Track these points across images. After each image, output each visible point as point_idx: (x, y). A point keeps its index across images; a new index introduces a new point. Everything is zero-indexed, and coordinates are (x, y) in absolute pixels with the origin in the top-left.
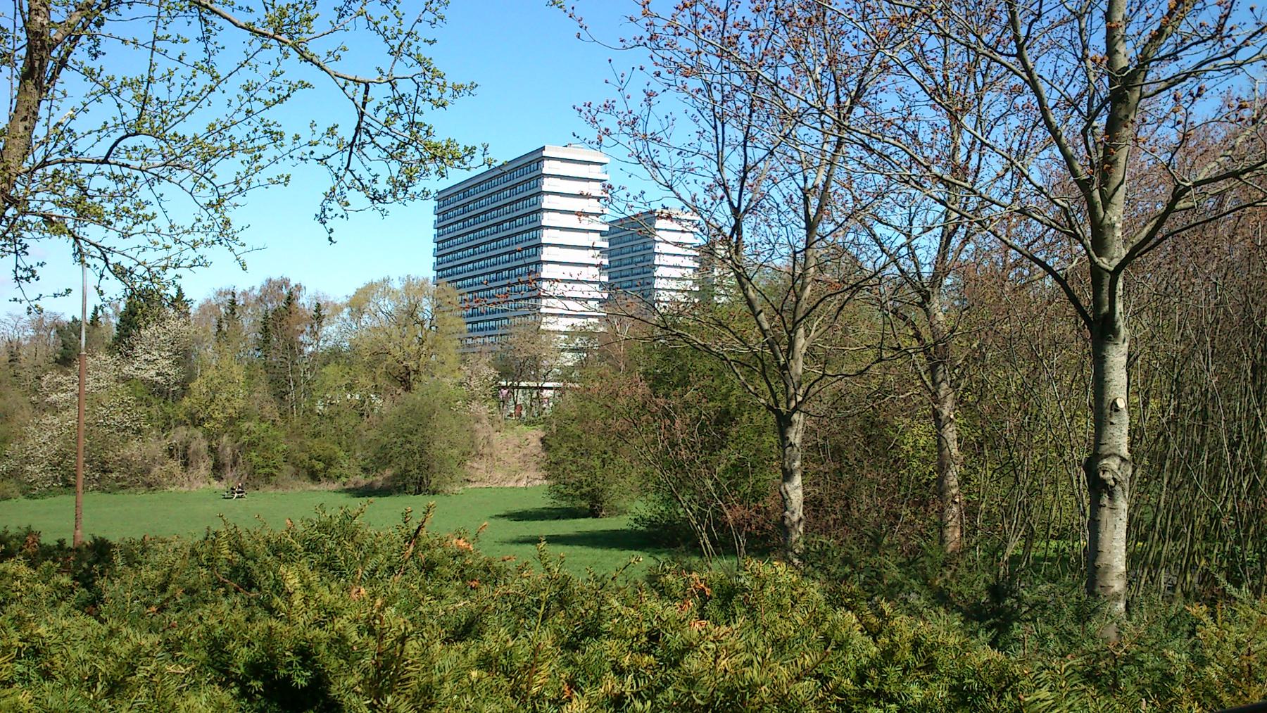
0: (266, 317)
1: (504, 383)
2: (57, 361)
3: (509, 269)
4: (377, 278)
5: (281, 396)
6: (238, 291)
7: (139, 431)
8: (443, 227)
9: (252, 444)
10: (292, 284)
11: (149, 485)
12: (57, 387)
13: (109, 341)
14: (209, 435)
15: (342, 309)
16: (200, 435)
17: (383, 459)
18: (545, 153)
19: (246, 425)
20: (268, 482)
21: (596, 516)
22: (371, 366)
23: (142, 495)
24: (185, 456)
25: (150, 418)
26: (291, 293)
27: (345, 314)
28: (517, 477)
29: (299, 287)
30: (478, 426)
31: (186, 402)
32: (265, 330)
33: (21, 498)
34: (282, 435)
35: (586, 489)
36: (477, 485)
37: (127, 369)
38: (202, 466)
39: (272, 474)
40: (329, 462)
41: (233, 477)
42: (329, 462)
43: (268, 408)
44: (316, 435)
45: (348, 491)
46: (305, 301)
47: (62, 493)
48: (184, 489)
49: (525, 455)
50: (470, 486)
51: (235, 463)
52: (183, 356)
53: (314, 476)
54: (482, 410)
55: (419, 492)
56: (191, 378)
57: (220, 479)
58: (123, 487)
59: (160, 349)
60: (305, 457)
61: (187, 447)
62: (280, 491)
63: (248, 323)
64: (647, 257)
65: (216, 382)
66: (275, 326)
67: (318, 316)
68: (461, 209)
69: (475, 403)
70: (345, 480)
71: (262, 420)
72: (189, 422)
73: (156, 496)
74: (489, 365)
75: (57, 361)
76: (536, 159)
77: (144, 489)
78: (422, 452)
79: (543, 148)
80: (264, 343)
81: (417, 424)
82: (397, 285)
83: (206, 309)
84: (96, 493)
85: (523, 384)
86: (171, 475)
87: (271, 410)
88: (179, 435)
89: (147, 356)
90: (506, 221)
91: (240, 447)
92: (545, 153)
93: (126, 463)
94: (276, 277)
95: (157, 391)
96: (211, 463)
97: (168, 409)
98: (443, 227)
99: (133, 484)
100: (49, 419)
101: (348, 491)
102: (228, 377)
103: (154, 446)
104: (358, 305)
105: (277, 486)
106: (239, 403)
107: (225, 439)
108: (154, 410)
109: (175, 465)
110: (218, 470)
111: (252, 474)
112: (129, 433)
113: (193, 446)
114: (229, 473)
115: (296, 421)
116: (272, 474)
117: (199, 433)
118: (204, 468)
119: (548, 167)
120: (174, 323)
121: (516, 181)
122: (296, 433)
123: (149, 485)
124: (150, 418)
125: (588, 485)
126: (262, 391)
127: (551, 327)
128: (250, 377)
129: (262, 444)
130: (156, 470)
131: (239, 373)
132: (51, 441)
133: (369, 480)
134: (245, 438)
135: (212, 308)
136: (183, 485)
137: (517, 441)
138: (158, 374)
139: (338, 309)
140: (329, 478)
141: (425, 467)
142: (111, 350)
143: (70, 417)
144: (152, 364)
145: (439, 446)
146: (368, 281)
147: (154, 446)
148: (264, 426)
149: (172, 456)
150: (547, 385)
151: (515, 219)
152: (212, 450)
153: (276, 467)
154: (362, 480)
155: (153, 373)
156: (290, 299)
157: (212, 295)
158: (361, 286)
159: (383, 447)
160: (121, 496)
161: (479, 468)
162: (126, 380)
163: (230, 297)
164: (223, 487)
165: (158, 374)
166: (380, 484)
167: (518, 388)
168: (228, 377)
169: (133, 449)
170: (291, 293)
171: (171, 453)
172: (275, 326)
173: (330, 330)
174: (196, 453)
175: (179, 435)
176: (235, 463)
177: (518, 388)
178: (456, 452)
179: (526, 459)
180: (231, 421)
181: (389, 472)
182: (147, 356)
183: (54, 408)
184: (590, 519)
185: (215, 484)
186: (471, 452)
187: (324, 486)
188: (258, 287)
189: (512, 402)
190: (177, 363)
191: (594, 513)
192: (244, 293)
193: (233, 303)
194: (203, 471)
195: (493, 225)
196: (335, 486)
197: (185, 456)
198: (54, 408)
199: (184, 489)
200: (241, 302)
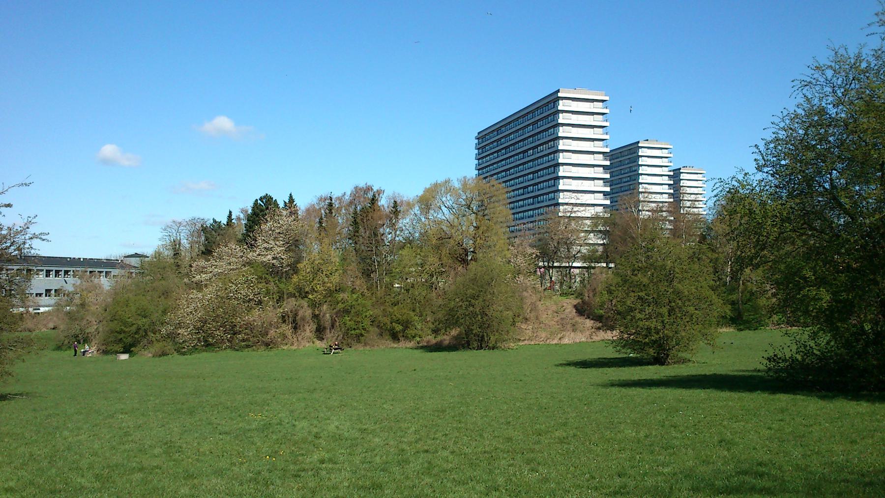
0: (355, 213)
1: (541, 264)
2: (203, 253)
3: (533, 185)
4: (441, 179)
5: (367, 274)
6: (334, 197)
7: (260, 302)
8: (482, 158)
9: (347, 312)
10: (375, 189)
11: (267, 345)
12: (202, 271)
13: (240, 237)
14: (313, 305)
15: (414, 205)
16: (306, 304)
17: (451, 320)
18: (560, 95)
19: (341, 296)
20: (359, 341)
21: (662, 364)
22: (438, 248)
23: (262, 352)
24: (294, 321)
25: (268, 293)
26: (374, 196)
27: (416, 210)
28: (559, 336)
29: (380, 192)
30: (525, 294)
31: (295, 279)
32: (355, 223)
33: (175, 354)
34: (369, 303)
35: (654, 337)
36: (526, 342)
37: (251, 255)
38: (308, 329)
39: (362, 335)
40: (407, 324)
41: (331, 337)
42: (407, 324)
43: (358, 282)
44: (395, 304)
45: (422, 348)
46: (384, 202)
47: (204, 351)
48: (294, 348)
49: (562, 319)
50: (521, 344)
51: (333, 326)
52: (294, 245)
53: (395, 337)
54: (530, 281)
55: (480, 348)
56: (299, 260)
57: (321, 339)
58: (248, 346)
59: (275, 239)
60: (387, 320)
61: (296, 315)
62: (368, 348)
63: (342, 220)
64: (633, 178)
65: (317, 262)
66: (362, 220)
67: (396, 210)
68: (495, 144)
69: (521, 278)
70: (418, 339)
71: (353, 291)
72: (297, 294)
73: (272, 353)
74: (532, 246)
75: (203, 253)
76: (553, 99)
77: (263, 348)
78: (484, 314)
79: (558, 91)
80: (354, 236)
81: (480, 289)
82: (457, 185)
83: (309, 211)
84: (228, 351)
85: (556, 264)
86: (284, 337)
87: (360, 284)
88: (289, 305)
89: (265, 245)
90: (530, 149)
91: (337, 313)
92: (560, 95)
93: (249, 326)
94: (362, 184)
95: (273, 271)
96: (315, 327)
97: (282, 286)
98: (482, 158)
99: (255, 343)
100: (195, 294)
101: (422, 348)
102: (324, 254)
103: (270, 314)
104: (426, 202)
105: (366, 344)
106: (336, 279)
107: (325, 307)
108: (272, 287)
109: (287, 329)
110: (320, 332)
111: (346, 333)
112: (252, 304)
113: (301, 313)
114: (328, 334)
115: (380, 292)
116: (362, 335)
117: (305, 303)
118: (309, 330)
119: (562, 105)
120: (285, 220)
121: (537, 118)
122: (380, 302)
123: (267, 345)
124: (268, 293)
125: (658, 333)
126: (354, 267)
127: (579, 214)
128: (344, 259)
129: (353, 311)
130: (272, 333)
131: (335, 257)
132: (196, 311)
133: (439, 338)
134: (340, 306)
135: (315, 210)
136: (292, 344)
137: (554, 308)
138: (274, 258)
139: (410, 205)
140: (406, 338)
141: (486, 326)
142: (240, 242)
143: (209, 293)
144: (268, 250)
145: (496, 310)
146: (433, 182)
147: (271, 313)
148: (355, 296)
149: (284, 322)
150: (575, 265)
151: (536, 147)
152: (315, 316)
153: (364, 329)
154: (432, 339)
155: (270, 257)
156: (374, 200)
157: (315, 201)
158: (428, 186)
159: (452, 310)
160: (246, 352)
161: (527, 329)
162: (249, 263)
163: (328, 201)
164: (324, 346)
165: (274, 258)
166: (447, 342)
167: (553, 267)
168: (324, 254)
169: (255, 316)
170: (374, 196)
171: (284, 319)
172: (362, 220)
173: (404, 222)
174: (303, 319)
175: (289, 305)
176: (333, 326)
177: (553, 267)
178: (510, 313)
179: (564, 322)
180: (330, 293)
181: (454, 332)
182: (265, 245)
183: (199, 286)
184: (657, 367)
185: (318, 343)
186: (519, 317)
187: (403, 344)
188: (348, 193)
189: (548, 277)
190: (288, 250)
191: (659, 361)
192: (338, 198)
193: (331, 205)
194: (308, 333)
195: (520, 153)
196: (412, 344)
197: (294, 321)
198: (199, 286)
199: (294, 348)
200: (336, 205)
